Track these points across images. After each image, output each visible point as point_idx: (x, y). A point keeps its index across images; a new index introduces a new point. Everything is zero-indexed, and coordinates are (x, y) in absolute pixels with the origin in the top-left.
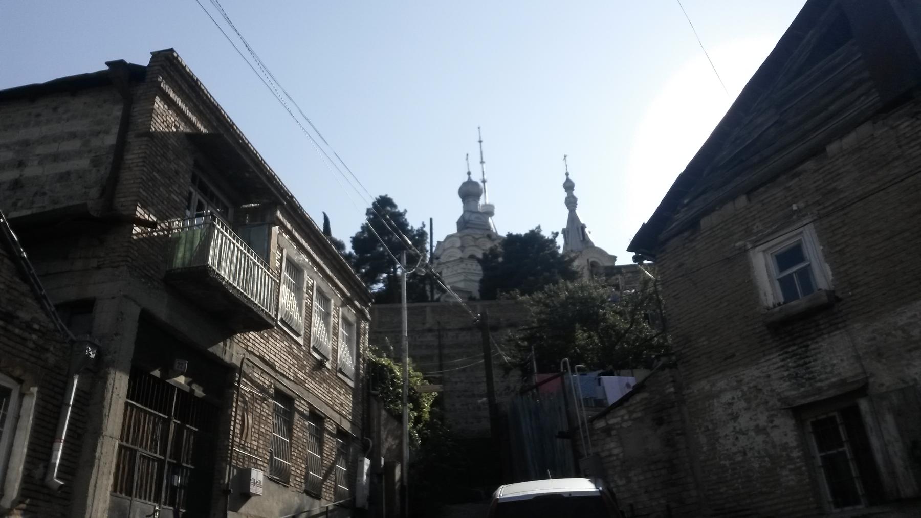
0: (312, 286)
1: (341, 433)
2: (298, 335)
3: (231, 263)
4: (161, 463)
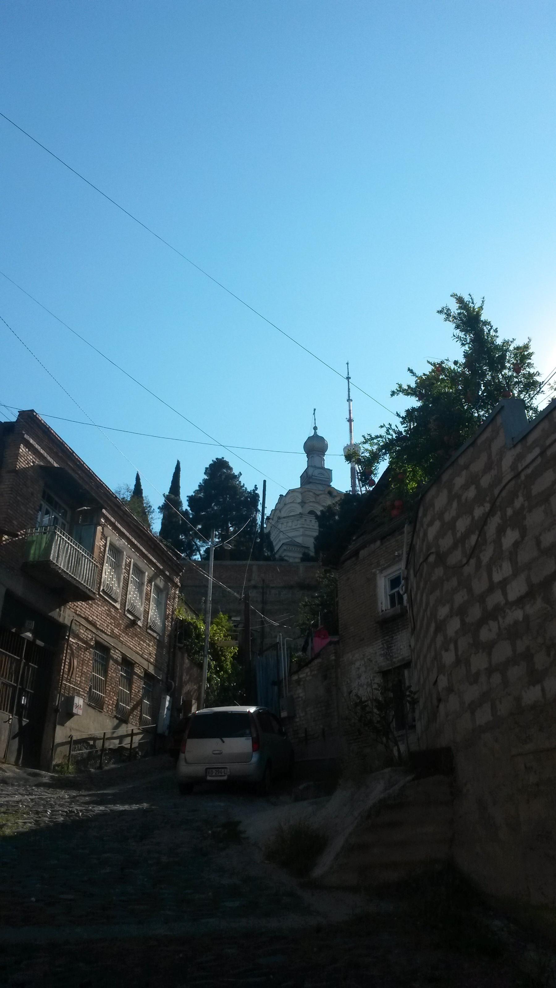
0: (130, 563)
1: (147, 675)
2: (116, 601)
3: (66, 557)
4: (14, 688)
